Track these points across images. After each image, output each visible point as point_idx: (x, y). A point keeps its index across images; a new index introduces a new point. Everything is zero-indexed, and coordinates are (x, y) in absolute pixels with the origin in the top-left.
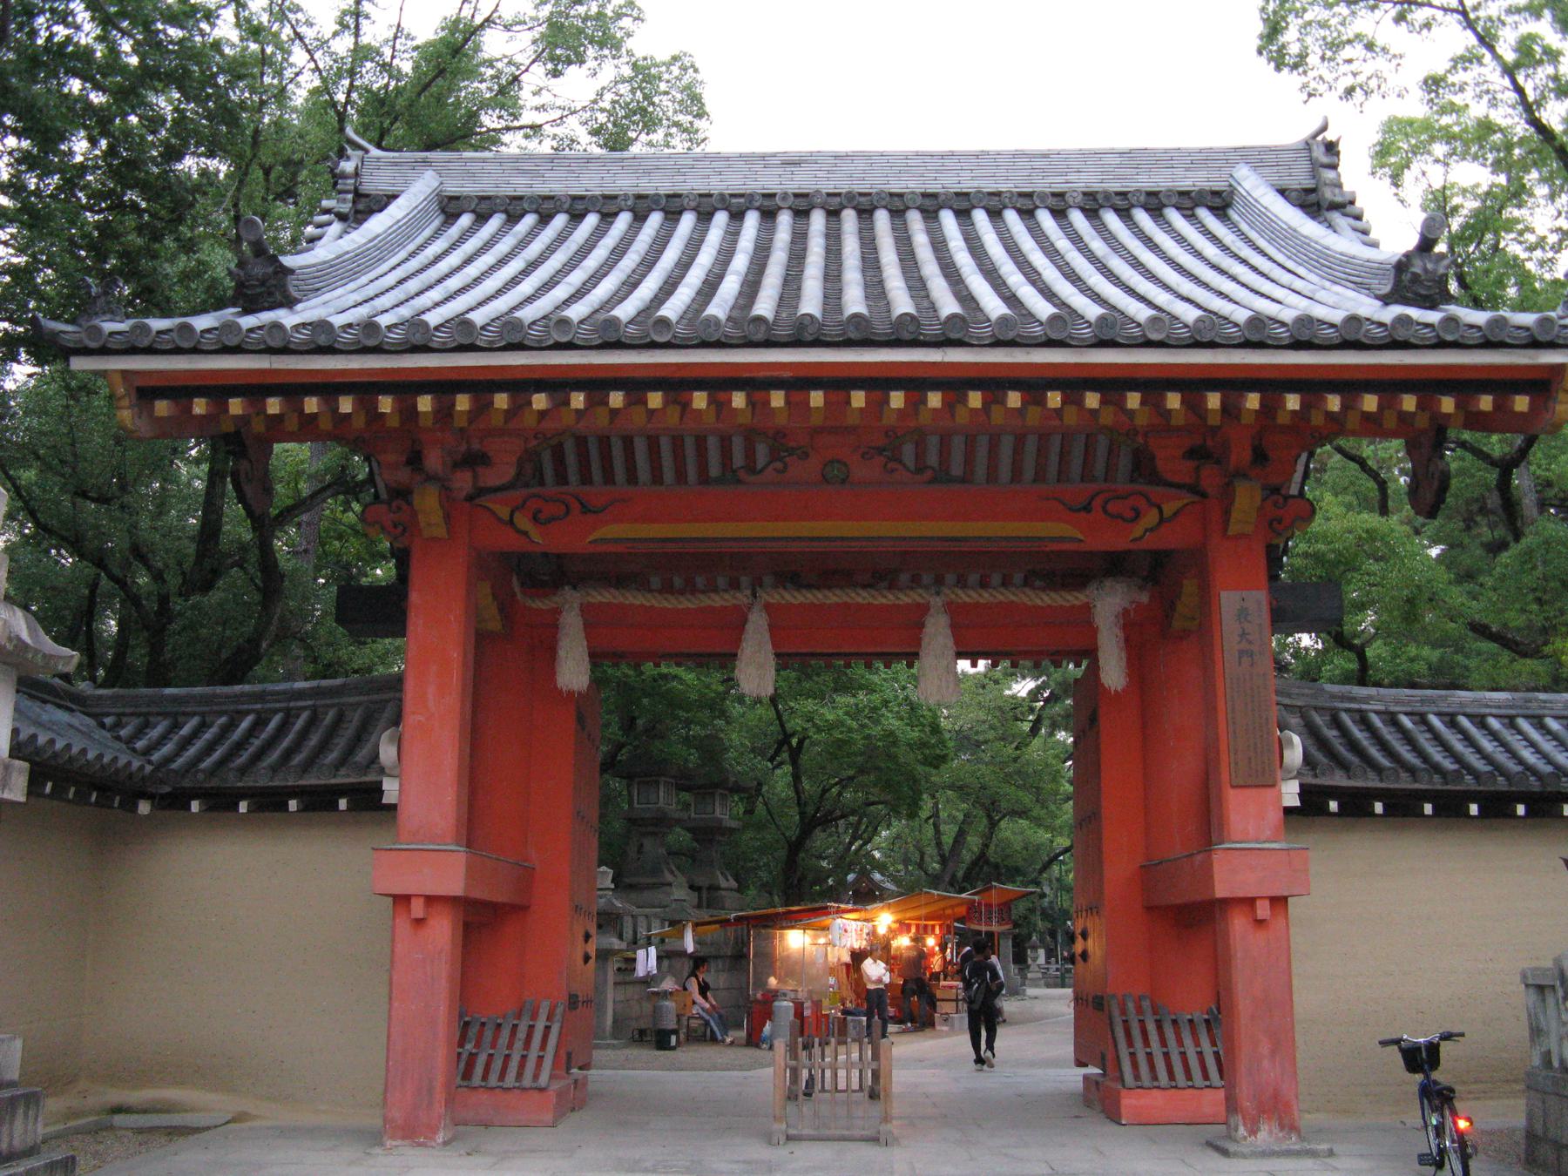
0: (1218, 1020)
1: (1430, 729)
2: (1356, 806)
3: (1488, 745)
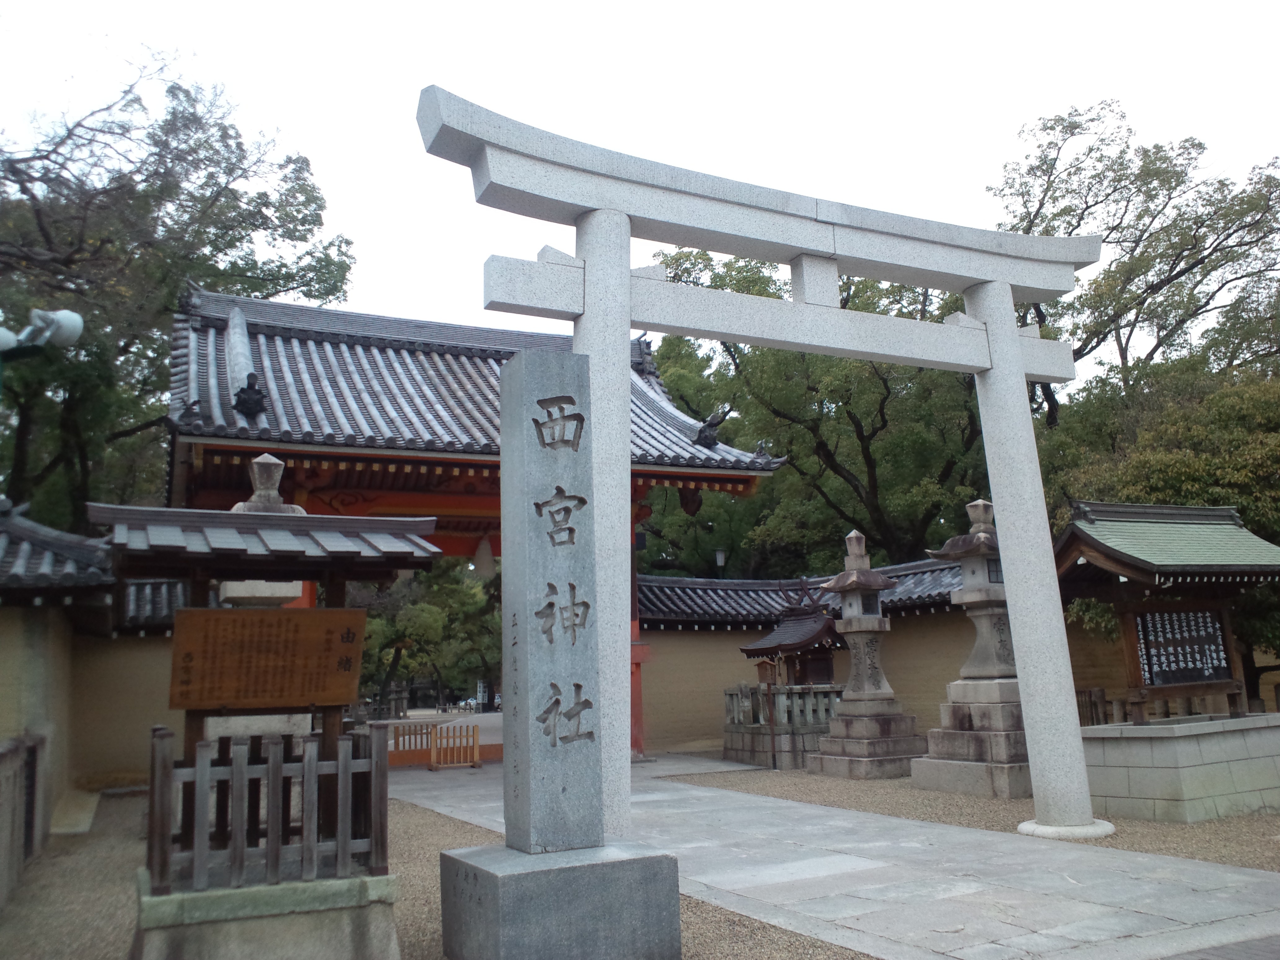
0: (1016, 798)
1: (677, 594)
3: (699, 601)
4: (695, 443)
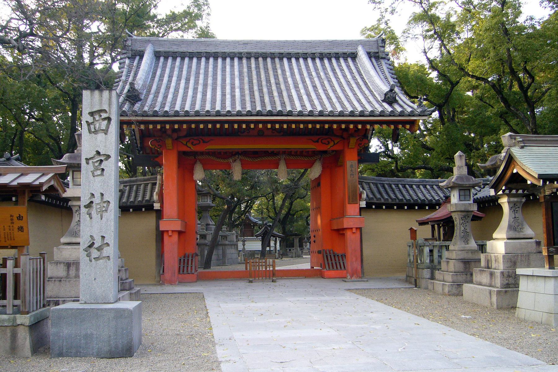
1: (399, 188)
2: (379, 207)
4: (383, 101)
